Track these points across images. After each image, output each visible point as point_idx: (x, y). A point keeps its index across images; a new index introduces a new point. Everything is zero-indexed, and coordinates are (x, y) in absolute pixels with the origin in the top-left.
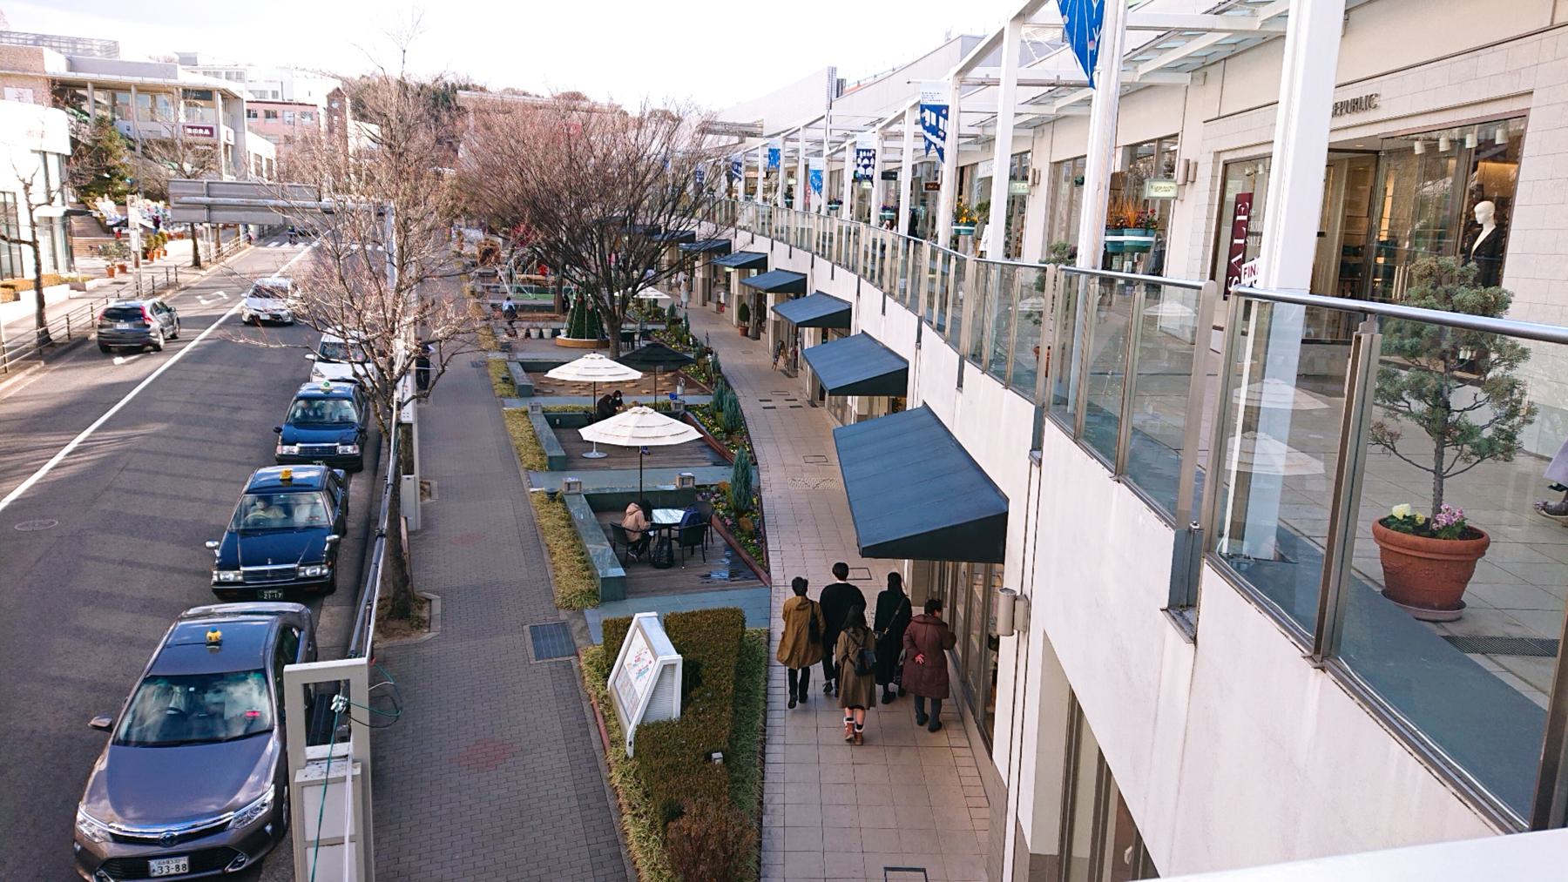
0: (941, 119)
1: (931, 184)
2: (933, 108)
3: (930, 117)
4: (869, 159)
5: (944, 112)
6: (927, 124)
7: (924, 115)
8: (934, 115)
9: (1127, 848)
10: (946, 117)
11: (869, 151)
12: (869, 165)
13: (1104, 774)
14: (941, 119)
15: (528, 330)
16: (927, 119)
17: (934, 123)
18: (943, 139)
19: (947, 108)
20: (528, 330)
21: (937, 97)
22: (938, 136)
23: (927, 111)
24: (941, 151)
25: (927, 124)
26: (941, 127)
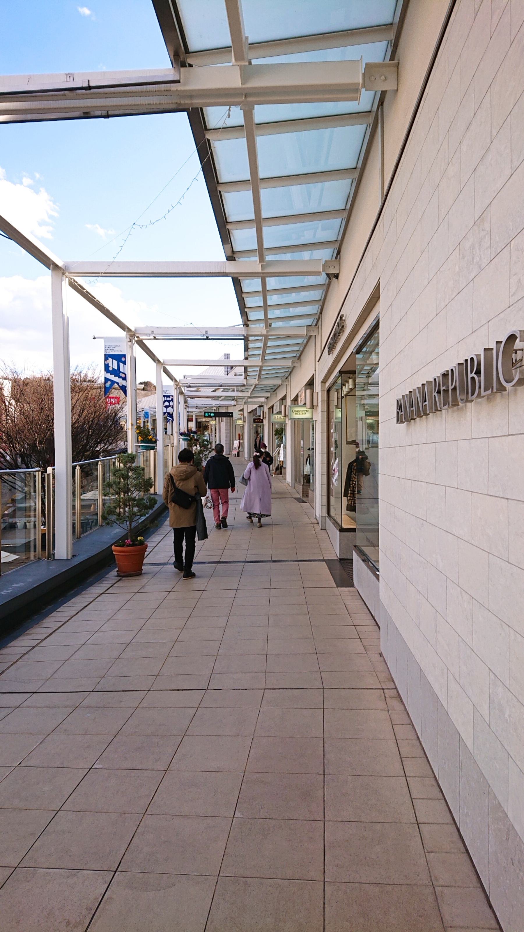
0: (121, 365)
1: (257, 419)
2: (114, 357)
3: (113, 364)
4: (169, 401)
5: (123, 359)
6: (111, 369)
7: (108, 362)
8: (115, 362)
9: (89, 9)
10: (124, 363)
11: (169, 396)
12: (169, 406)
13: (376, 327)
14: (121, 365)
15: (25, 523)
16: (110, 365)
17: (116, 368)
18: (125, 379)
19: (124, 356)
20: (25, 523)
21: (117, 349)
22: (120, 377)
23: (110, 360)
24: (124, 389)
25: (111, 369)
26: (121, 370)
